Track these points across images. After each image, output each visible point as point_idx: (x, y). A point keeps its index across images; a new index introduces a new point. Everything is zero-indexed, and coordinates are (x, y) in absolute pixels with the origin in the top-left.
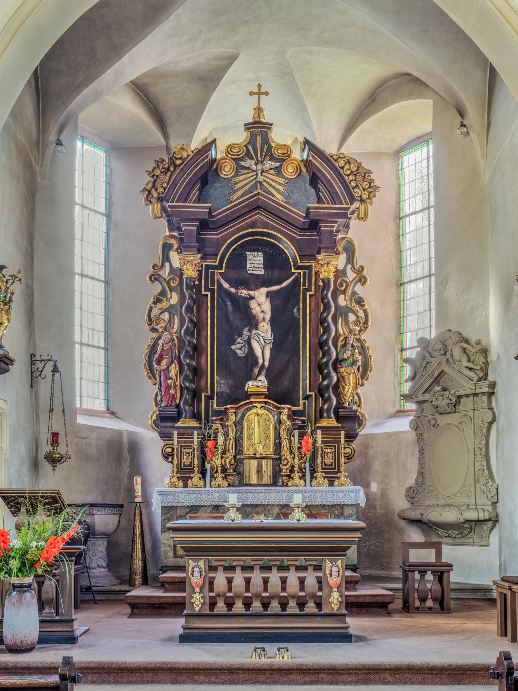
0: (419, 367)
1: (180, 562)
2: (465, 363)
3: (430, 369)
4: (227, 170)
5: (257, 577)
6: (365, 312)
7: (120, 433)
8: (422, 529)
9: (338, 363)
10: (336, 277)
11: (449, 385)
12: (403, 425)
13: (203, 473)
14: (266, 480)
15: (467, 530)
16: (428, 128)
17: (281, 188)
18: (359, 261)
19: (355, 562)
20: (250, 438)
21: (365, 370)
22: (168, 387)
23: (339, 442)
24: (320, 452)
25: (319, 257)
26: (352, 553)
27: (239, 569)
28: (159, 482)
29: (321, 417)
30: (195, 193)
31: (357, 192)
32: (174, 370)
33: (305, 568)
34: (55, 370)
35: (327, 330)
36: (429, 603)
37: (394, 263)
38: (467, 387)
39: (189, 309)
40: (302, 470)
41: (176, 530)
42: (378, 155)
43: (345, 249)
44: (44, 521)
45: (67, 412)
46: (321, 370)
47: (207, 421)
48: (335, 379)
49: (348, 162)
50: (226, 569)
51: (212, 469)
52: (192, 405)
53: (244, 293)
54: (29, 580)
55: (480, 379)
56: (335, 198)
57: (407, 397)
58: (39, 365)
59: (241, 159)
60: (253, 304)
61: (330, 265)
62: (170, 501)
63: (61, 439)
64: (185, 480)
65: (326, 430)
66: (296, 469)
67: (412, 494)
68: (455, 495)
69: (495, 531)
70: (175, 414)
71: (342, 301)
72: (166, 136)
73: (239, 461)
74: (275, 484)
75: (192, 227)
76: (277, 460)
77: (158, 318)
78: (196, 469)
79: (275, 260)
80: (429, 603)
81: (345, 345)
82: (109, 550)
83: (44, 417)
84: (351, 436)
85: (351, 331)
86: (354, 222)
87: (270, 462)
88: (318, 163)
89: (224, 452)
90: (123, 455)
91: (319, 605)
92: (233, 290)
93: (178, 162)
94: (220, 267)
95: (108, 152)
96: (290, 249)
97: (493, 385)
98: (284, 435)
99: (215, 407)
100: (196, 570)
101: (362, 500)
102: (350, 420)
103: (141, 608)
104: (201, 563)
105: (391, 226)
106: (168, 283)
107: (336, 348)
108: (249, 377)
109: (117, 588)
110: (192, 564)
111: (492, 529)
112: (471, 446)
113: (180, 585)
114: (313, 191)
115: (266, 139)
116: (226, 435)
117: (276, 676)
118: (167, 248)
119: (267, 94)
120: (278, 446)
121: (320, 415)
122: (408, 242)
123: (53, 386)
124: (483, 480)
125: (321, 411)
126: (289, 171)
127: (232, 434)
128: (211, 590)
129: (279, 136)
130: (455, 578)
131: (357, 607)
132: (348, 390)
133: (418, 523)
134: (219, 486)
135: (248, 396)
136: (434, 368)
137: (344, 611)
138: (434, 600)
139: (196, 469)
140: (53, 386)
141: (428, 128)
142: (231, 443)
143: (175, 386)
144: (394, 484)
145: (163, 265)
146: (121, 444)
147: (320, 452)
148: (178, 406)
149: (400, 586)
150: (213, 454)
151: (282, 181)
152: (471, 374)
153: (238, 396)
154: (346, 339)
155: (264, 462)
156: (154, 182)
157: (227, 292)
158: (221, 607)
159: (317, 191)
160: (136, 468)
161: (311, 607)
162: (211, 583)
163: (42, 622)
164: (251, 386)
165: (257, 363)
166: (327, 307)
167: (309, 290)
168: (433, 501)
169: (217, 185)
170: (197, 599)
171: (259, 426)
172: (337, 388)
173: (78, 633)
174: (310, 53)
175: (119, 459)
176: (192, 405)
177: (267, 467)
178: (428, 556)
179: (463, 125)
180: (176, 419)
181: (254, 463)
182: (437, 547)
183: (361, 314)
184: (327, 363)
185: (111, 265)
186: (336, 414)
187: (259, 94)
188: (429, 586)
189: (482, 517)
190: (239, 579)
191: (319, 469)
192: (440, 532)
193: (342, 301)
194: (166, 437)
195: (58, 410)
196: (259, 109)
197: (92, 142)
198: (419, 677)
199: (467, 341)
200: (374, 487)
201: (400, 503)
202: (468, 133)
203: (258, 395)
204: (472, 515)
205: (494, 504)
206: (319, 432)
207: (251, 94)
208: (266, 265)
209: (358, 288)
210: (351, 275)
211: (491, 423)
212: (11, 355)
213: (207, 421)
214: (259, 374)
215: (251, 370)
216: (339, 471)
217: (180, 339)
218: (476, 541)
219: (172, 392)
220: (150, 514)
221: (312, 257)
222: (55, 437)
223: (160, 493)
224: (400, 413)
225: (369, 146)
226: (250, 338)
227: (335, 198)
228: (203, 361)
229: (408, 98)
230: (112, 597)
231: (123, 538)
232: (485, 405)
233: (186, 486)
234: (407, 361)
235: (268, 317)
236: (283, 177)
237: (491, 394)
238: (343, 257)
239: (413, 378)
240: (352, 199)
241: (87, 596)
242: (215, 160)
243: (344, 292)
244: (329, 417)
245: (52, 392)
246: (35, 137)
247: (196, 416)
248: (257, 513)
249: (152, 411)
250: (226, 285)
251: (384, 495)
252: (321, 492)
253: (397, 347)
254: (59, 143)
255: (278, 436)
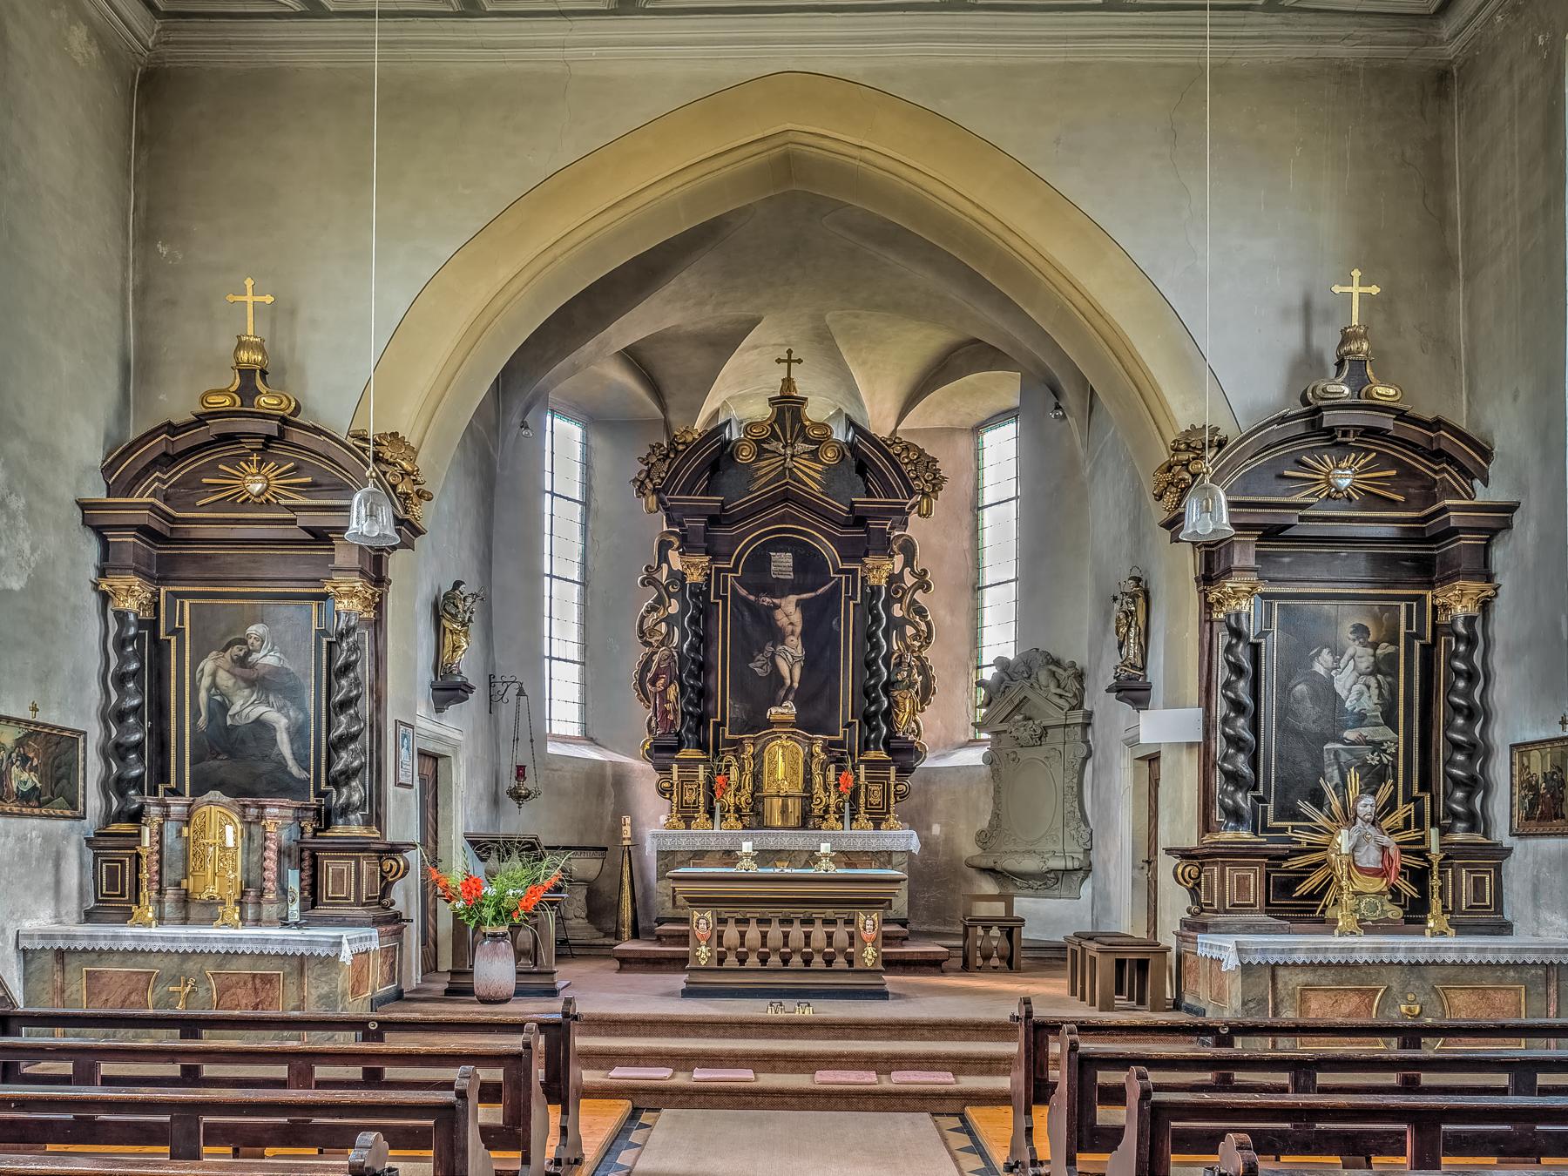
0: (995, 693)
1: (682, 913)
2: (1053, 689)
3: (1010, 694)
4: (746, 455)
5: (775, 932)
6: (928, 624)
7: (602, 764)
8: (996, 879)
9: (889, 686)
10: (889, 583)
11: (1034, 713)
12: (973, 757)
13: (711, 812)
14: (792, 822)
15: (1050, 881)
16: (1014, 401)
17: (817, 476)
18: (918, 566)
19: (905, 916)
20: (773, 772)
21: (927, 692)
22: (666, 712)
23: (888, 779)
24: (863, 789)
25: (867, 560)
26: (900, 904)
27: (753, 922)
28: (653, 821)
29: (867, 748)
30: (703, 483)
31: (917, 485)
32: (673, 692)
33: (833, 922)
34: (521, 693)
35: (876, 646)
36: (995, 962)
37: (970, 563)
38: (1054, 716)
39: (694, 621)
40: (839, 810)
41: (675, 879)
42: (951, 431)
43: (902, 549)
44: (515, 866)
45: (537, 739)
46: (867, 695)
47: (716, 752)
48: (886, 704)
49: (906, 448)
50: (760, 921)
51: (722, 808)
52: (697, 733)
53: (767, 600)
54: (503, 929)
55: (1073, 708)
56: (889, 491)
57: (979, 726)
58: (501, 688)
59: (764, 441)
60: (779, 615)
61: (879, 568)
62: (669, 845)
63: (529, 772)
64: (688, 821)
65: (871, 764)
66: (832, 809)
67: (983, 839)
68: (1039, 840)
69: (1088, 884)
70: (675, 743)
71: (897, 611)
72: (664, 409)
73: (757, 800)
74: (804, 826)
75: (700, 523)
76: (808, 798)
77: (652, 631)
78: (702, 809)
79: (808, 563)
80: (995, 962)
81: (899, 664)
82: (588, 898)
83: (505, 748)
84: (905, 770)
85: (908, 647)
86: (913, 517)
87: (798, 802)
88: (866, 448)
89: (738, 789)
90: (608, 788)
91: (850, 963)
92: (752, 598)
93: (681, 447)
94: (734, 569)
95: (585, 428)
96: (829, 551)
97: (1090, 715)
98: (816, 769)
99: (727, 735)
100: (702, 922)
101: (915, 845)
102: (904, 754)
103: (628, 963)
104: (708, 915)
105: (967, 518)
106: (666, 588)
107: (888, 668)
108: (774, 702)
109: (600, 942)
110: (697, 915)
111: (1083, 880)
112: (1059, 783)
113: (683, 939)
114: (860, 479)
115: (797, 416)
116: (741, 769)
117: (796, 1030)
118: (664, 546)
119: (799, 361)
120: (808, 782)
121: (866, 745)
122: (987, 537)
123: (518, 712)
124: (1073, 824)
125: (867, 742)
126: (829, 456)
127: (749, 767)
128: (720, 944)
129: (816, 411)
130: (1028, 934)
131: (893, 964)
132: (903, 717)
133: (991, 872)
134: (732, 828)
135: (770, 724)
136: (1015, 694)
137: (880, 967)
138: (1001, 958)
139: (702, 809)
140: (518, 712)
141: (1014, 401)
142: (748, 778)
143: (675, 711)
144: (962, 826)
145: (659, 566)
146: (603, 776)
147: (863, 789)
148: (678, 734)
149: (960, 943)
150: (724, 791)
151: (819, 467)
152: (1061, 702)
153: (756, 723)
154: (900, 656)
155: (790, 801)
156: (649, 471)
157: (745, 600)
158: (731, 962)
159: (866, 480)
160: (623, 805)
161: (840, 963)
162: (720, 937)
163: (518, 973)
164: (773, 712)
165: (784, 684)
166: (877, 619)
167: (853, 598)
168: (1012, 847)
169: (732, 471)
170: (704, 954)
171: (783, 761)
172: (888, 715)
173: (559, 986)
174: (857, 317)
175: (601, 794)
176: (697, 733)
177: (794, 807)
178: (998, 909)
179: (1058, 407)
180: (676, 749)
181: (777, 802)
182: (1008, 900)
183: (924, 627)
184: (875, 686)
185: (589, 563)
186: (886, 744)
187: (789, 361)
188: (995, 943)
189: (1070, 865)
190: (753, 933)
191: (862, 810)
192: (1019, 882)
193: (897, 611)
194: (664, 769)
195: (525, 738)
196: (788, 382)
197: (564, 416)
198: (962, 1034)
199: (1057, 663)
200: (936, 829)
201: (968, 848)
202: (1064, 416)
203: (783, 723)
204: (1058, 864)
205: (1087, 851)
206: (862, 767)
207: (779, 361)
208: (797, 568)
209: (919, 596)
210: (909, 580)
211: (1085, 759)
212: (470, 682)
213: (716, 752)
214: (785, 698)
215: (776, 692)
216: (888, 812)
217: (680, 654)
218: (1064, 893)
219: (671, 717)
220: (641, 858)
221: (857, 558)
222: (520, 772)
223: (655, 836)
224: (973, 743)
225: (937, 421)
226: (773, 654)
227: (889, 491)
228: (711, 682)
229: (989, 369)
230: (594, 951)
231: (605, 886)
232: (1079, 737)
233: (688, 827)
234: (980, 684)
235: (798, 629)
236: (821, 462)
237: (1086, 726)
238: (899, 560)
239: (987, 704)
240: (912, 493)
241: (567, 950)
242: (730, 441)
243: (900, 600)
244: (877, 749)
245: (517, 719)
246: (493, 422)
247: (702, 746)
248: (780, 860)
249: (646, 739)
250: (743, 592)
251: (948, 840)
252: (861, 836)
253: (972, 664)
254: (524, 425)
255: (808, 771)
